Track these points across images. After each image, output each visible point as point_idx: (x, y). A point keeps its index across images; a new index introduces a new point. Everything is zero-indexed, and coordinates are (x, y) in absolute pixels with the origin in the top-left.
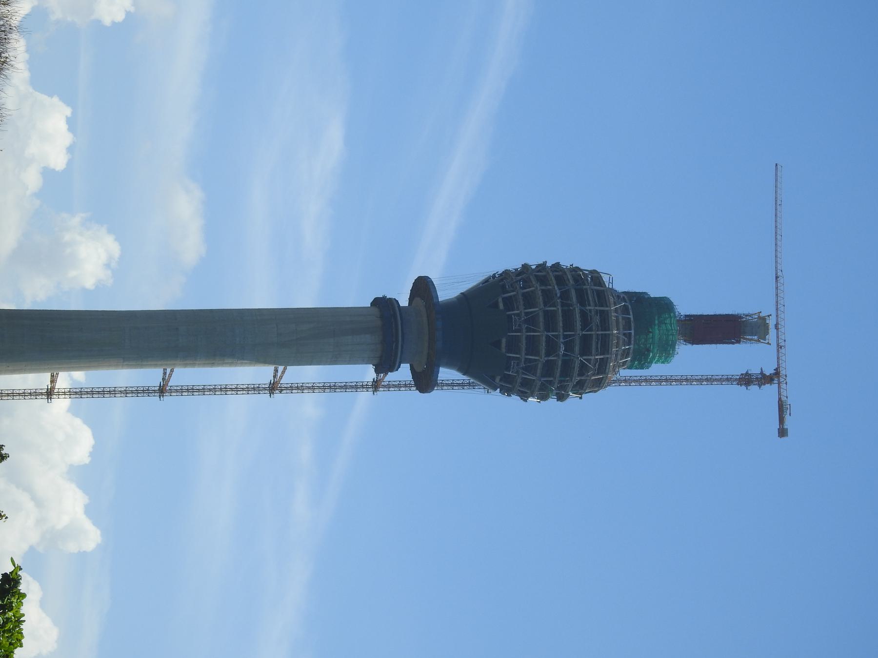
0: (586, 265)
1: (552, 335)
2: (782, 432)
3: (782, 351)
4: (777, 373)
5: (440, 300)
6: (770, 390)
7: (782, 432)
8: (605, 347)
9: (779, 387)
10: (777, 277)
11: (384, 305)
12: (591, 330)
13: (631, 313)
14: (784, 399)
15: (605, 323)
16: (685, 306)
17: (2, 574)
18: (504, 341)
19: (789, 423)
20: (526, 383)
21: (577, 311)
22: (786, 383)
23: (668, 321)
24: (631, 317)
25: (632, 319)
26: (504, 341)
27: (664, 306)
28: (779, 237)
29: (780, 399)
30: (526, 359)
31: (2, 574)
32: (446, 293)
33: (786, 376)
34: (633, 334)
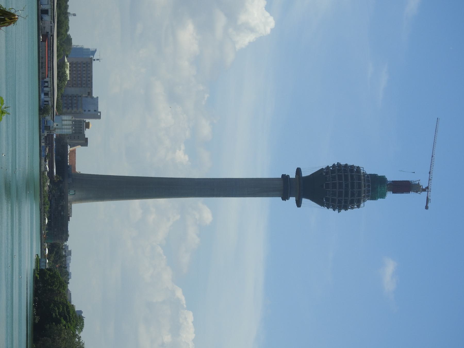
0: (356, 165)
1: (340, 199)
2: (427, 208)
3: (431, 181)
4: (427, 188)
5: (303, 176)
6: (424, 194)
7: (427, 208)
8: (359, 195)
9: (428, 193)
10: (432, 156)
11: (285, 177)
12: (354, 197)
13: (370, 182)
14: (429, 197)
15: (360, 187)
16: (390, 178)
17: (97, 97)
18: (324, 184)
19: (429, 205)
20: (333, 171)
21: (350, 192)
22: (430, 191)
23: (383, 189)
24: (370, 179)
25: (370, 180)
26: (324, 184)
27: (382, 180)
28: (435, 144)
29: (427, 197)
30: (332, 198)
31: (97, 97)
32: (305, 173)
33: (431, 189)
34: (370, 195)
